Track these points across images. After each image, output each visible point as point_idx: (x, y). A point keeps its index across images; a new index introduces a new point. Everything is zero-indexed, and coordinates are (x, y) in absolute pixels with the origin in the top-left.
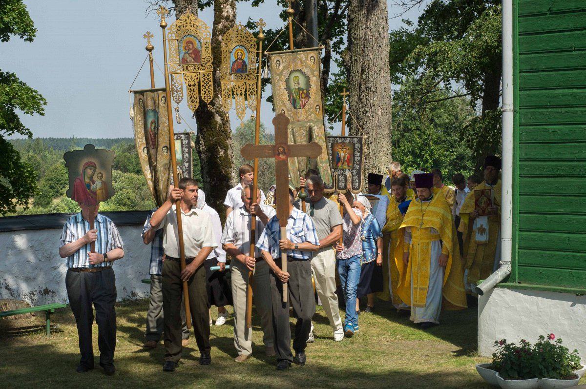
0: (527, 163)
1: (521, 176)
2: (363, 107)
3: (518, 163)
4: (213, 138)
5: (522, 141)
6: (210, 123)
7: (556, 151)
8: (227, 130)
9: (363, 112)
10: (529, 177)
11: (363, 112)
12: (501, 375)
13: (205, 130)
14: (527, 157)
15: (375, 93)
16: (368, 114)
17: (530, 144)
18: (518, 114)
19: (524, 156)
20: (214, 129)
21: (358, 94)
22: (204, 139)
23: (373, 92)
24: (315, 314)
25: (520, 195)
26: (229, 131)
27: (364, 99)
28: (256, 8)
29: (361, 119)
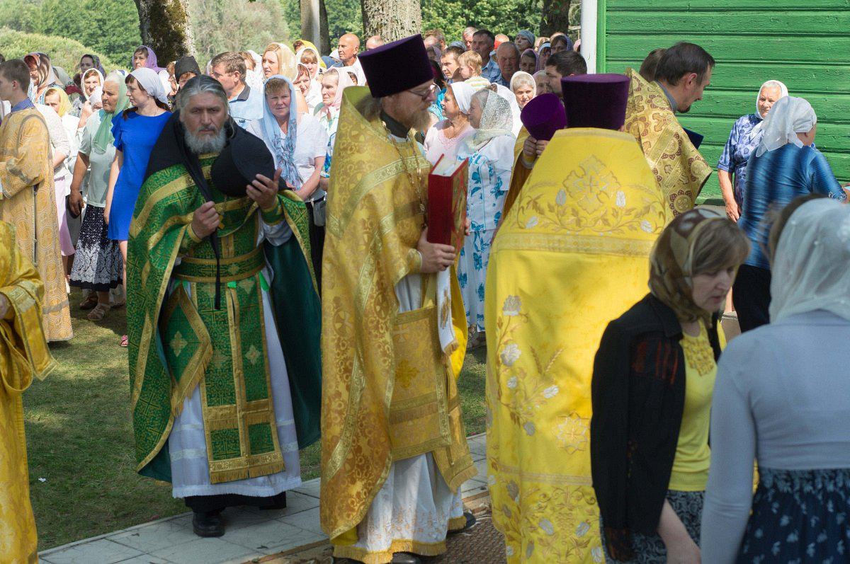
3: (605, 14)
25: (607, 60)
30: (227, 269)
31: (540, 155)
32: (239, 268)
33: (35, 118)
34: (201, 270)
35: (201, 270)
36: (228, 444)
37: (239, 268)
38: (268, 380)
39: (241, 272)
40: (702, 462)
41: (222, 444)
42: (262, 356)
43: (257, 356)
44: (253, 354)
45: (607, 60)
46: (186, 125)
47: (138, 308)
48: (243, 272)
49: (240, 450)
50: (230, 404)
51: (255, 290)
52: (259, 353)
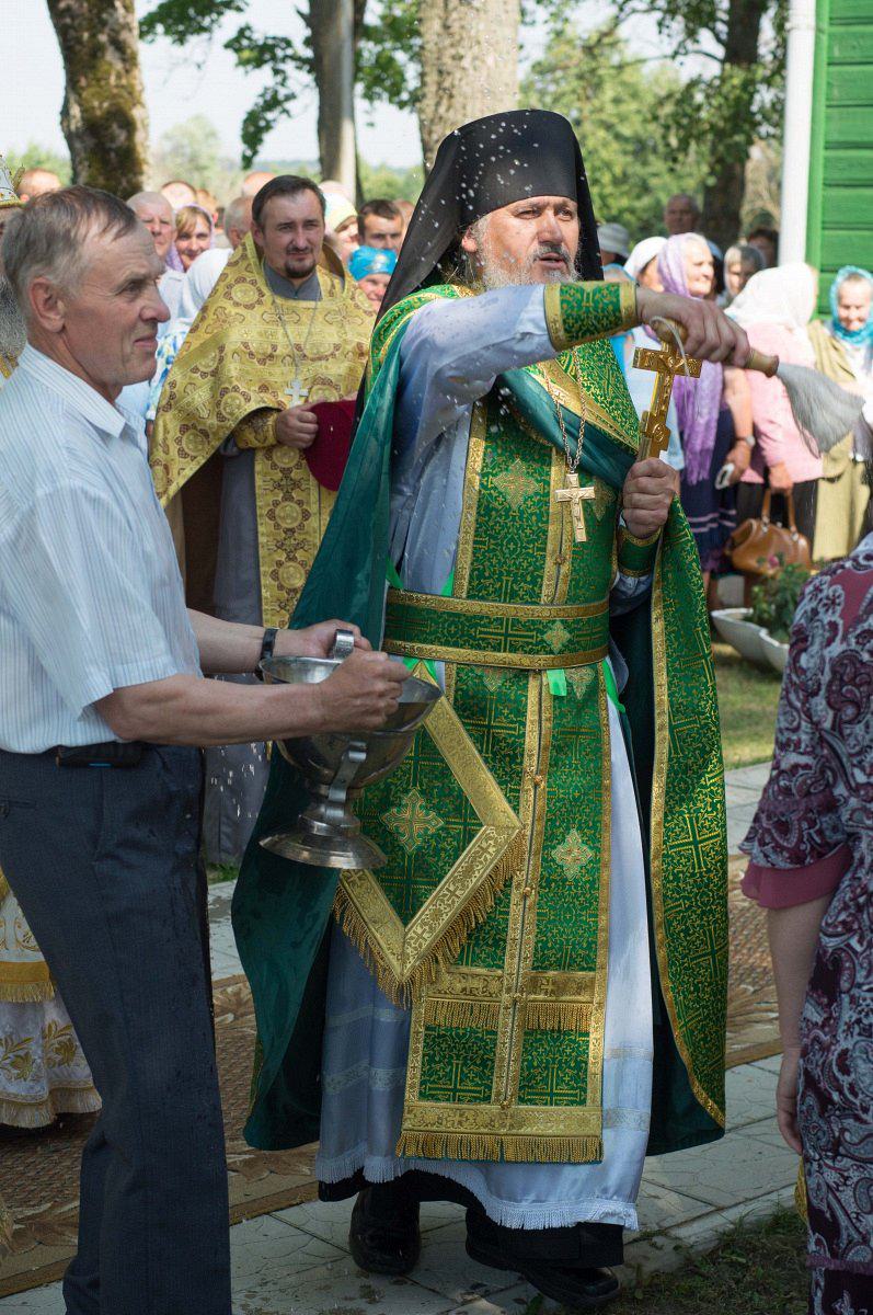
0: (841, 153)
1: (828, 185)
2: (452, 45)
3: (822, 153)
4: (101, 103)
5: (833, 100)
6: (93, 68)
7: (17, 645)
8: (132, 86)
9: (454, 58)
10: (846, 186)
11: (454, 58)
12: (771, 634)
13: (83, 82)
14: (842, 138)
15: (482, 14)
16: (466, 63)
17: (850, 110)
18: (825, 38)
19: (836, 137)
20: (103, 83)
21: (442, 14)
22: (80, 105)
23: (478, 10)
24: (318, 1139)
25: (824, 228)
26: (138, 88)
27: (455, 28)
28: (251, 24)
29: (449, 73)
30: (543, 633)
31: (148, 118)
32: (568, 636)
33: (269, 205)
34: (476, 632)
35: (476, 632)
36: (465, 1064)
37: (568, 636)
38: (602, 924)
39: (570, 646)
40: (119, 415)
41: (450, 1063)
42: (595, 861)
43: (584, 861)
44: (572, 852)
45: (824, 228)
46: (139, 125)
47: (710, 984)
48: (575, 650)
49: (490, 1088)
50: (488, 966)
51: (594, 691)
52: (591, 853)
